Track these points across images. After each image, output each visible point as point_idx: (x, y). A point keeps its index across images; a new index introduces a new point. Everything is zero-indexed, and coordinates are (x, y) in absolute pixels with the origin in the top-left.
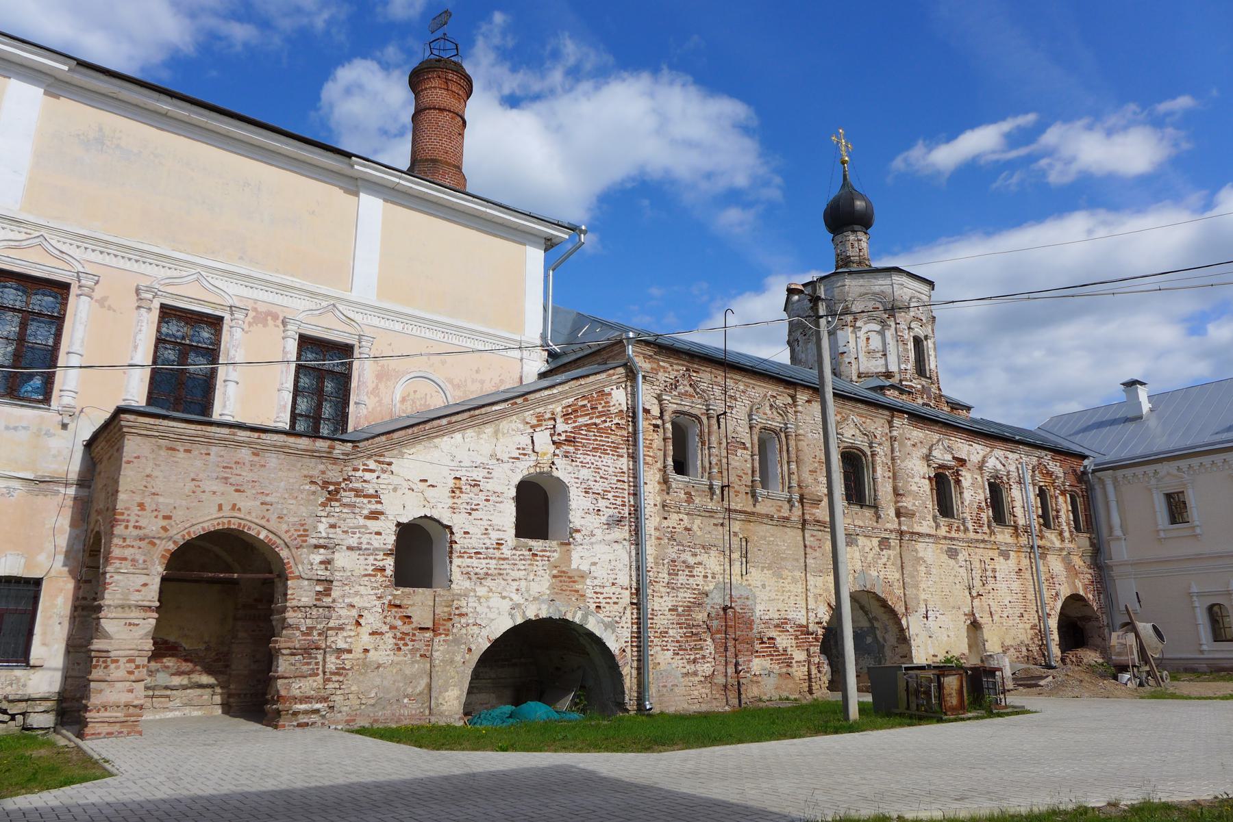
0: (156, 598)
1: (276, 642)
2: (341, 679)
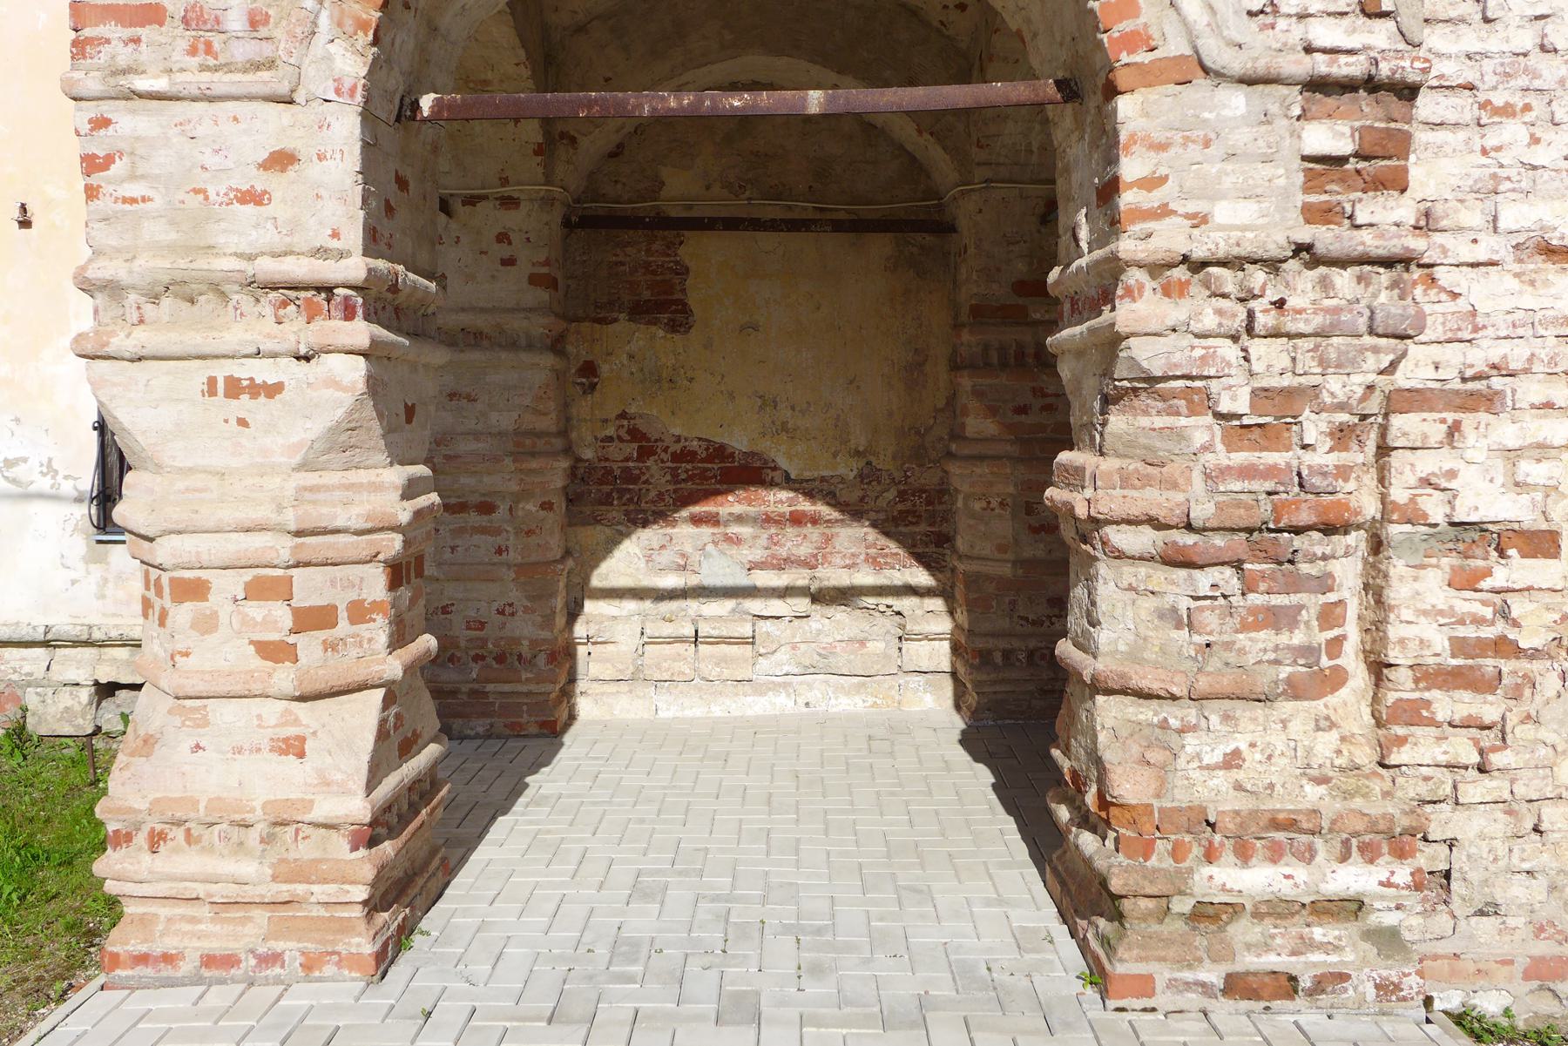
0: (354, 236)
1: (1076, 477)
2: (1489, 708)
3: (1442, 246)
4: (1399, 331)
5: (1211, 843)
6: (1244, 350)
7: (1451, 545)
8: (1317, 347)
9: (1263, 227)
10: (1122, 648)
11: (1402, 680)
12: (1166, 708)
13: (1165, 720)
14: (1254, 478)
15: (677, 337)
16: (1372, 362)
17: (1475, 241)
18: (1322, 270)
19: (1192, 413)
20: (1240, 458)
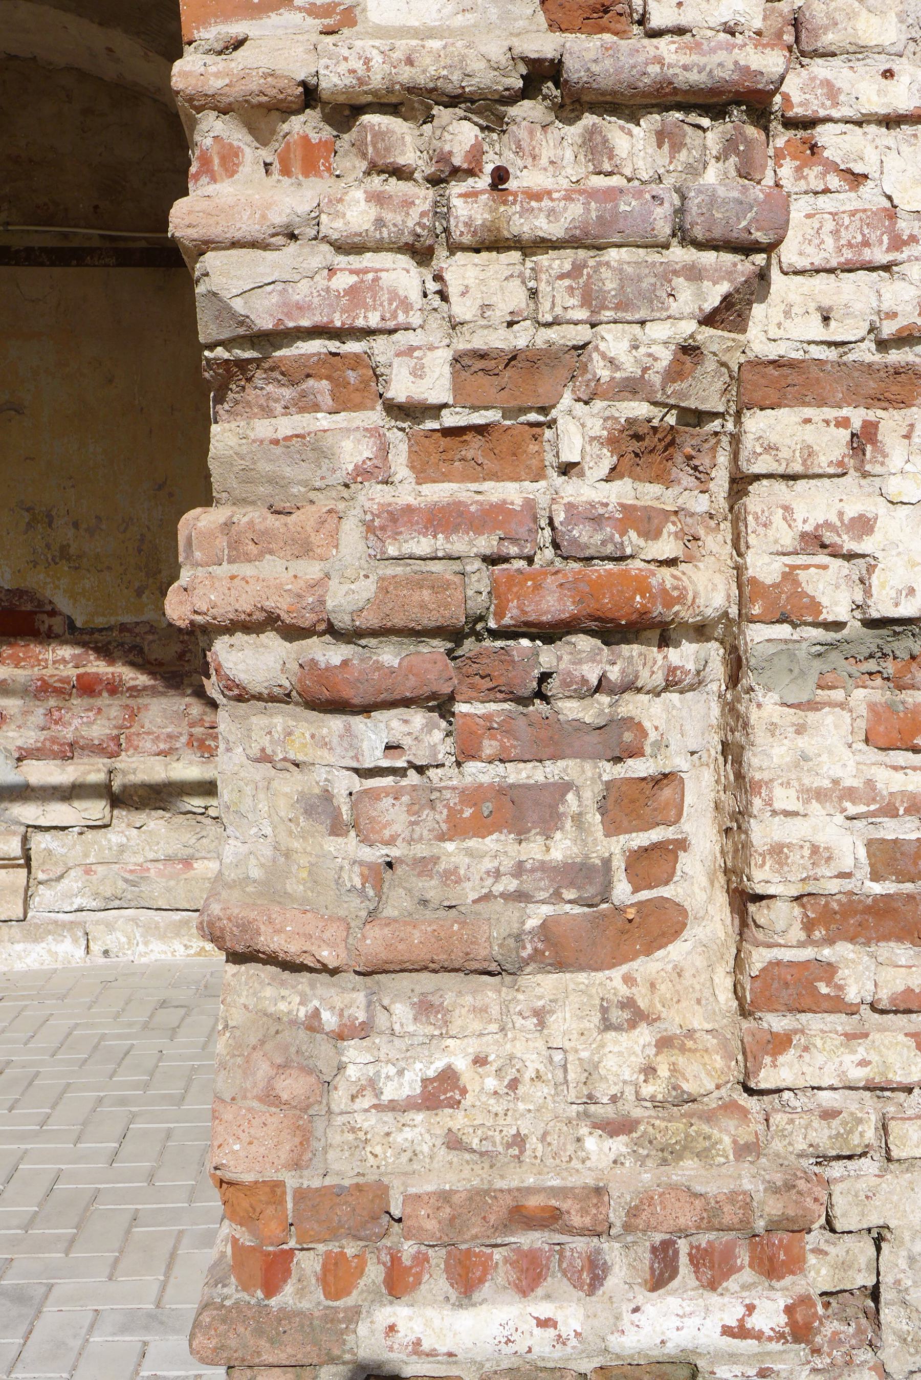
3: (828, 84)
5: (395, 1259)
6: (438, 278)
7: (872, 665)
8: (577, 270)
9: (461, 32)
10: (255, 873)
11: (780, 926)
12: (320, 991)
13: (316, 1013)
14: (456, 529)
16: (696, 297)
17: (888, 74)
18: (589, 119)
20: (439, 492)
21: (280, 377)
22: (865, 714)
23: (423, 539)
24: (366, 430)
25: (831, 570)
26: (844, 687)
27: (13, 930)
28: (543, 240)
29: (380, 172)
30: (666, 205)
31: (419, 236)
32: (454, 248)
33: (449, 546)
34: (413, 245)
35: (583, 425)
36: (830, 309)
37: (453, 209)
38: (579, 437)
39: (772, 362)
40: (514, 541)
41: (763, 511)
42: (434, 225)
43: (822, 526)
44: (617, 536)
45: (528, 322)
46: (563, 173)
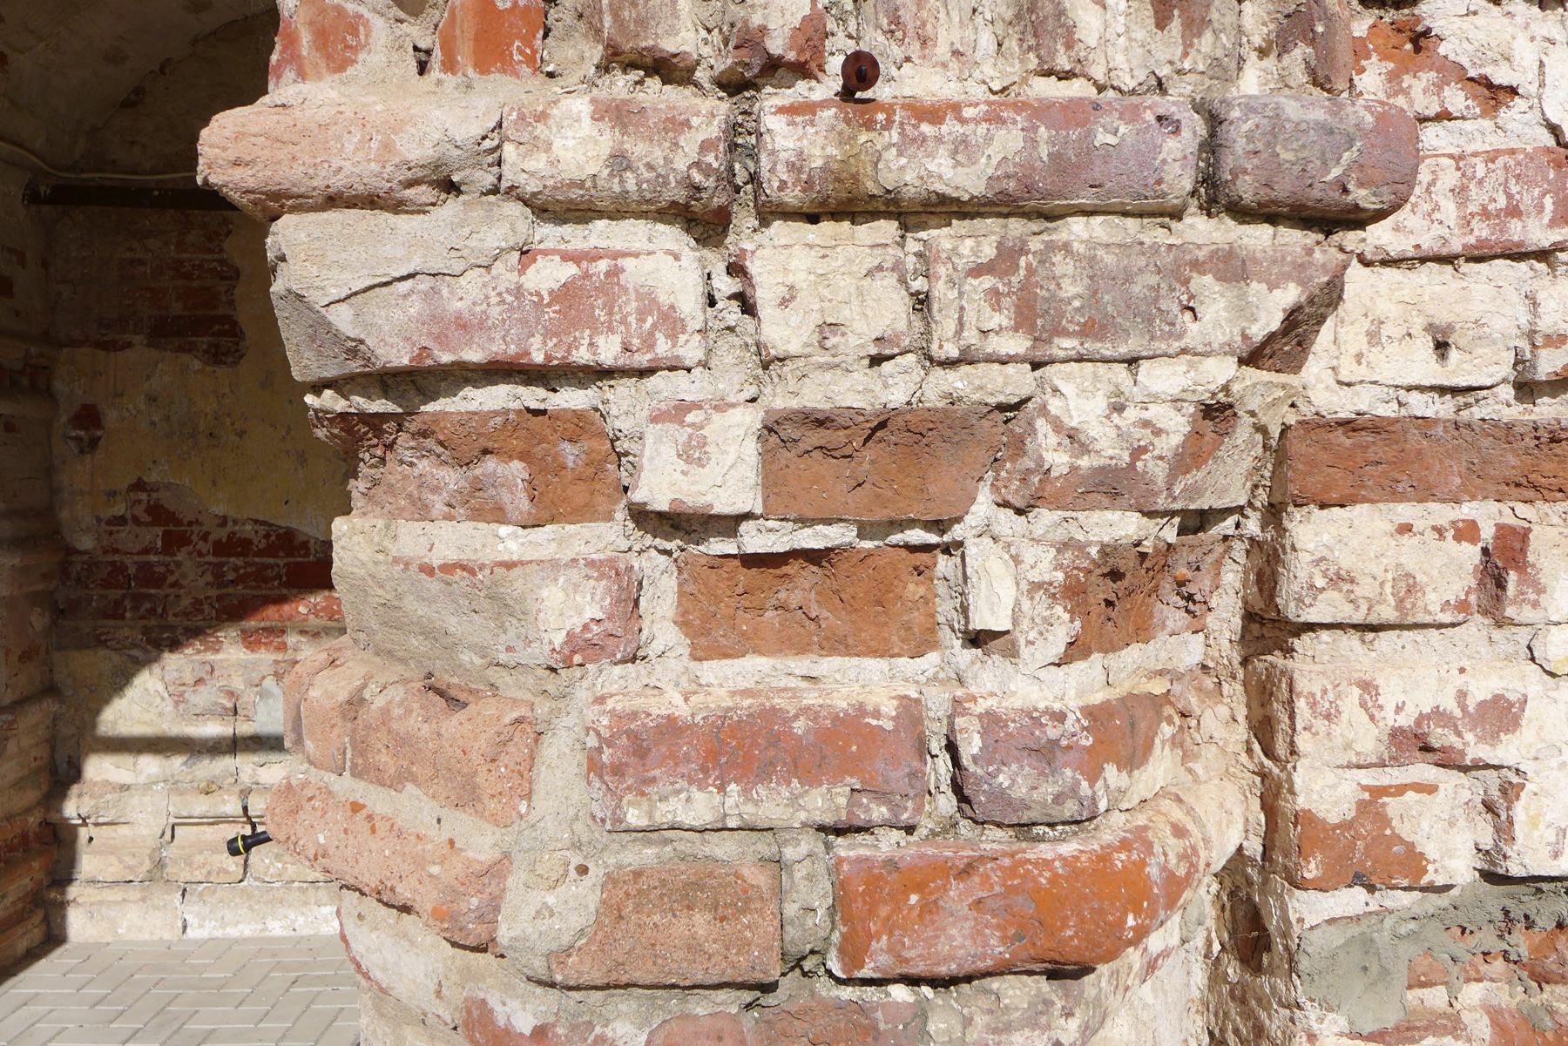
4: (1321, 192)
6: (736, 269)
8: (1008, 257)
14: (764, 772)
15: (221, 371)
16: (1226, 316)
19: (547, 508)
20: (736, 680)
21: (440, 450)
22: (1487, 1038)
23: (698, 795)
24: (591, 564)
25: (1441, 793)
26: (1446, 983)
27: (320, 892)
28: (943, 199)
29: (628, 66)
30: (1186, 133)
31: (698, 189)
32: (768, 213)
33: (749, 809)
34: (687, 206)
35: (1016, 560)
36: (1450, 328)
37: (767, 137)
38: (1009, 583)
39: (1344, 424)
40: (880, 795)
41: (1325, 692)
42: (731, 169)
43: (1428, 717)
44: (1085, 784)
45: (911, 357)
46: (977, 74)
